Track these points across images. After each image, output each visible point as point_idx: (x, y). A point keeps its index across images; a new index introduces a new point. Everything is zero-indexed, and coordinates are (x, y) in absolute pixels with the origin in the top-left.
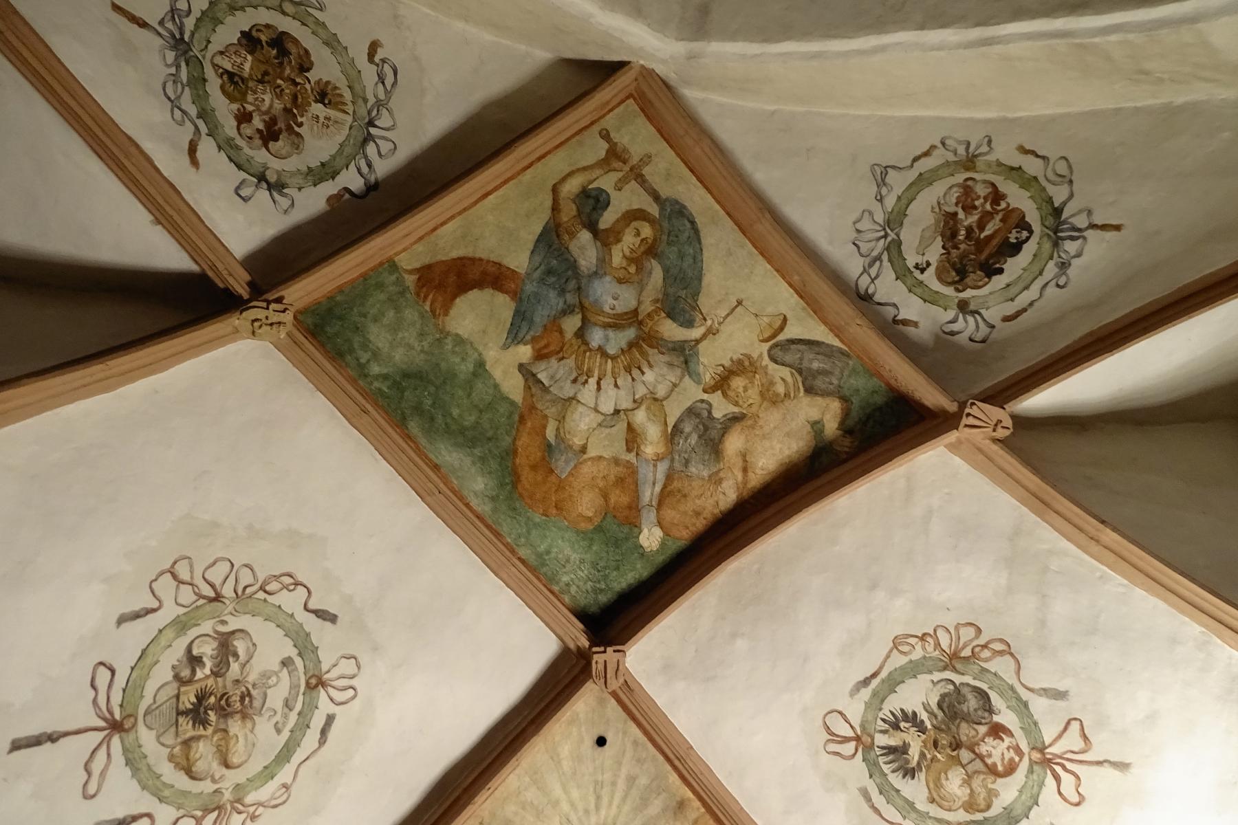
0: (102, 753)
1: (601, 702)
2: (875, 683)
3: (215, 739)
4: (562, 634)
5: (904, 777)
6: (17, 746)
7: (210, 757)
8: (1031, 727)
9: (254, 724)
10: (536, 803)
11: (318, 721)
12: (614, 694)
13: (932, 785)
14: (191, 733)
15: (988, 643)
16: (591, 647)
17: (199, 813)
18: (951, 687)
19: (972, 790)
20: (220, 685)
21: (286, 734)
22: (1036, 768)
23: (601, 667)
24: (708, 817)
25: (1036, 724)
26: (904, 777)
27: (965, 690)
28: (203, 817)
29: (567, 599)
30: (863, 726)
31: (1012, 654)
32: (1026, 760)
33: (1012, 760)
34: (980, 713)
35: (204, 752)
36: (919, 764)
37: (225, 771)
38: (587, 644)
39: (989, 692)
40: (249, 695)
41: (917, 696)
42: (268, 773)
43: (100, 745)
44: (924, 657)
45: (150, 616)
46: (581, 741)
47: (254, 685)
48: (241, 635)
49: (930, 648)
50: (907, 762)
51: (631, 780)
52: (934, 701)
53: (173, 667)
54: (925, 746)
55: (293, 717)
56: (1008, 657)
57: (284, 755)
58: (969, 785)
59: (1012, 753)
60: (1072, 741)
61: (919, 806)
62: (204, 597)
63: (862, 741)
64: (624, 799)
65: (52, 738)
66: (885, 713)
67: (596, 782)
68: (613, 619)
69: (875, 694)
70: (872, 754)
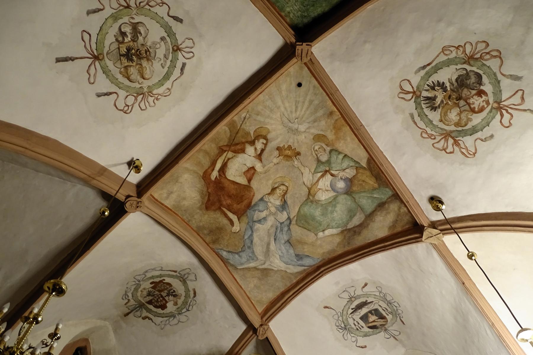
0: (93, 67)
1: (301, 68)
2: (428, 68)
3: (137, 67)
4: (284, 36)
5: (431, 110)
6: (58, 60)
7: (136, 74)
8: (498, 92)
9: (152, 63)
10: (270, 106)
11: (179, 65)
12: (305, 64)
13: (443, 114)
14: (127, 64)
15: (491, 51)
16: (296, 42)
17: (136, 95)
18: (465, 72)
19: (460, 118)
20: (136, 45)
21: (166, 69)
22: (493, 110)
23: (300, 52)
24: (342, 119)
25: (500, 91)
26: (431, 110)
27: (471, 74)
28: (137, 96)
29: (288, 20)
30: (418, 88)
31: (500, 58)
32: (490, 107)
33: (483, 106)
34: (475, 85)
35: (133, 71)
36: (439, 106)
37: (143, 80)
38: (294, 41)
39: (483, 75)
40: (149, 51)
41: (447, 75)
42: (161, 83)
43: (91, 64)
44: (456, 57)
45: (100, 12)
46: (291, 84)
47: (150, 47)
48: (142, 25)
49: (460, 53)
50: (434, 104)
51: (311, 102)
52: (454, 78)
53: (115, 36)
54: (444, 98)
55: (168, 63)
56: (498, 59)
57: (167, 77)
58: (460, 116)
59: (484, 103)
60: (516, 100)
61: (434, 123)
62: (122, 6)
63: (416, 94)
64: (307, 109)
65: (72, 59)
66: (430, 82)
67: (296, 101)
68: (308, 31)
69: (427, 73)
70: (419, 100)
